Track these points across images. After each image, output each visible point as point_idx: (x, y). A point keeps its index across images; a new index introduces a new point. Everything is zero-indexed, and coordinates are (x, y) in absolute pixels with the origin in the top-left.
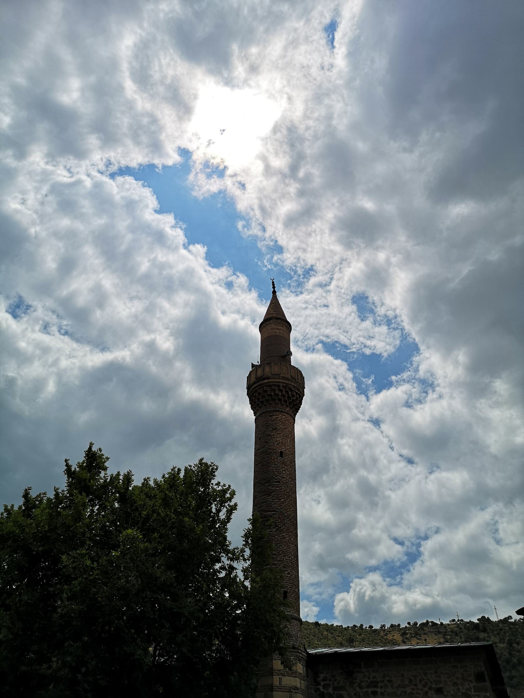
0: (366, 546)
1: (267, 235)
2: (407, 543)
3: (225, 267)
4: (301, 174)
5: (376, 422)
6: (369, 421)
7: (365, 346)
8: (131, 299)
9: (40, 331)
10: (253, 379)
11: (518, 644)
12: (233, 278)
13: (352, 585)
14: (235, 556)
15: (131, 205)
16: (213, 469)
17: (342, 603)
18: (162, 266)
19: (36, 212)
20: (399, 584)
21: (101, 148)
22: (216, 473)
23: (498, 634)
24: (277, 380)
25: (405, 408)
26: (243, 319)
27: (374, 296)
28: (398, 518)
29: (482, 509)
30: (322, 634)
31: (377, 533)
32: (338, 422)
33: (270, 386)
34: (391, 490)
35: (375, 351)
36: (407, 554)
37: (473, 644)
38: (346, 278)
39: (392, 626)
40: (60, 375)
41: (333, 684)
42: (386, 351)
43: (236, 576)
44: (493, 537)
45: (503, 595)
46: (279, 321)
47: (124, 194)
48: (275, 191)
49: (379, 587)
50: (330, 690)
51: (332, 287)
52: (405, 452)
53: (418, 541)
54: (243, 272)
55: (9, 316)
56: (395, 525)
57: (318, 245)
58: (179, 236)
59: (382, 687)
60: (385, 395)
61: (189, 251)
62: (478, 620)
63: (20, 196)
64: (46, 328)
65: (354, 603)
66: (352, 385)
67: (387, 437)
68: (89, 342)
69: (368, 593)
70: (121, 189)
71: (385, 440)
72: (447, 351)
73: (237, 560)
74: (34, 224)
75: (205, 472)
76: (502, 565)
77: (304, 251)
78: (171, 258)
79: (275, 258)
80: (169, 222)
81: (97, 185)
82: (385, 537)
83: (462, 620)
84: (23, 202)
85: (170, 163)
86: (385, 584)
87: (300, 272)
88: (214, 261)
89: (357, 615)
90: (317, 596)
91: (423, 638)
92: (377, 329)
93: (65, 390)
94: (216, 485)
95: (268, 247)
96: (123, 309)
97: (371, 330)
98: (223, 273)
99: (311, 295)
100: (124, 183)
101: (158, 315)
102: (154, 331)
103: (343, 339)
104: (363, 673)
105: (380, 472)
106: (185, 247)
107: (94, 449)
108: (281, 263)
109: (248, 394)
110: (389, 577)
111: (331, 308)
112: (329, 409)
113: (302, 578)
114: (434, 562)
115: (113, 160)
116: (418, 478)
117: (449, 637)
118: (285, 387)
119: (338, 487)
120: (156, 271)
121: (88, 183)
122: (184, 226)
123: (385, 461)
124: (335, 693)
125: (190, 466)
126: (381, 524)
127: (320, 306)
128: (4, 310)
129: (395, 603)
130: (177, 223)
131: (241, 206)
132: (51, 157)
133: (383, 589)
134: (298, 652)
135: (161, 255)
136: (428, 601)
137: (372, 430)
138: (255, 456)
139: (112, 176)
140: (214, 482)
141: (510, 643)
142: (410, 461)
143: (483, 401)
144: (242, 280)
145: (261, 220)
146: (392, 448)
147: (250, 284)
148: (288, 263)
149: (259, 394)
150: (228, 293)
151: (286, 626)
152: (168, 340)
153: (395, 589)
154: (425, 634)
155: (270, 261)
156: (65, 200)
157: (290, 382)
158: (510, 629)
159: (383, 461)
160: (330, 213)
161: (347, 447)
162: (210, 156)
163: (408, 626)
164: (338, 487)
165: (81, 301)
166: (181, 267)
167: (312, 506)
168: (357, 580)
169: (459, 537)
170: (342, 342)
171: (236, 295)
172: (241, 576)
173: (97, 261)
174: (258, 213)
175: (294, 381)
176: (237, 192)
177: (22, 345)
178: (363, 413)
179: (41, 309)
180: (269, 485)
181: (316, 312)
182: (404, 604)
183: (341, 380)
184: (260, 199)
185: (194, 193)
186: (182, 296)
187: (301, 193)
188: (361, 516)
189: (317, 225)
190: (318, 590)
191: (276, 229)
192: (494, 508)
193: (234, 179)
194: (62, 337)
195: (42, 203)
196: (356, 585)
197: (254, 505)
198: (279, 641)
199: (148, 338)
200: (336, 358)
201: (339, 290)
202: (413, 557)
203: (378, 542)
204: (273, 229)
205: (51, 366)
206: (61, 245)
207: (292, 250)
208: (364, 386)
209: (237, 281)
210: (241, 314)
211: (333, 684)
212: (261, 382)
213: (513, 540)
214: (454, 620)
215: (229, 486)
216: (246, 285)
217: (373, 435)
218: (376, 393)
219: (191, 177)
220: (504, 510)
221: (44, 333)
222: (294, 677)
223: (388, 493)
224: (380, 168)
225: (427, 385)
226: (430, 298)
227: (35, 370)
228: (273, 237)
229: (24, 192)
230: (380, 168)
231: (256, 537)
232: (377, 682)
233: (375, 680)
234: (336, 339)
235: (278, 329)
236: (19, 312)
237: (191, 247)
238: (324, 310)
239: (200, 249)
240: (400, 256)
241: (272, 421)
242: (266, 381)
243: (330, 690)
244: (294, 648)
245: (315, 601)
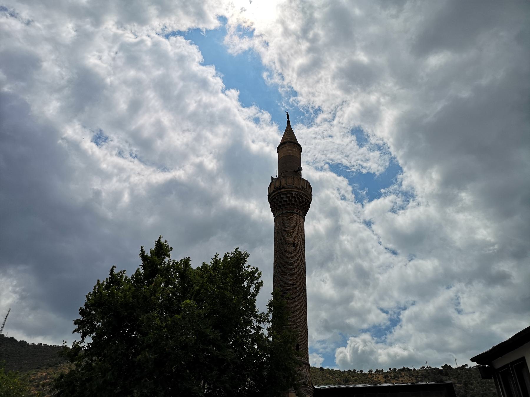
0: (360, 314)
1: (285, 83)
2: (390, 312)
3: (253, 106)
4: (311, 35)
5: (368, 224)
6: (363, 223)
7: (362, 167)
8: (184, 131)
9: (116, 155)
10: (273, 189)
11: (472, 384)
12: (259, 115)
13: (348, 342)
14: (262, 319)
15: (181, 59)
16: (245, 256)
17: (341, 355)
18: (207, 106)
19: (110, 65)
20: (384, 342)
21: (158, 16)
22: (247, 259)
23: (457, 377)
25: (390, 213)
26: (268, 145)
27: (367, 129)
28: (384, 294)
29: (448, 288)
30: (325, 376)
31: (369, 305)
32: (340, 223)
33: (286, 194)
34: (379, 273)
35: (370, 171)
36: (391, 320)
37: (438, 383)
38: (346, 116)
39: (377, 371)
40: (132, 190)
42: (378, 171)
43: (262, 333)
44: (455, 309)
45: (462, 350)
47: (177, 51)
48: (291, 47)
49: (369, 344)
51: (335, 122)
52: (390, 246)
53: (399, 311)
54: (266, 110)
55: (94, 145)
56: (382, 298)
57: (323, 90)
58: (218, 83)
60: (376, 203)
61: (227, 95)
62: (442, 367)
63: (97, 54)
64: (120, 154)
65: (350, 355)
66: (351, 196)
67: (376, 235)
68: (153, 164)
69: (361, 348)
70: (174, 47)
71: (375, 237)
72: (424, 169)
73: (263, 322)
74: (109, 74)
75: (238, 259)
76: (461, 328)
77: (313, 94)
78: (213, 100)
79: (291, 100)
80: (210, 73)
81: (156, 44)
82: (374, 307)
83: (430, 367)
84: (100, 58)
85: (212, 27)
86: (373, 342)
87: (311, 111)
88: (244, 102)
89: (352, 364)
90: (322, 350)
91: (400, 380)
92: (372, 154)
93: (137, 201)
94: (247, 267)
95: (286, 92)
96: (178, 139)
97: (367, 155)
98: (252, 111)
99: (319, 128)
100: (176, 42)
101: (204, 144)
102: (202, 156)
103: (345, 162)
105: (371, 260)
106: (223, 92)
108: (296, 104)
109: (269, 201)
110: (376, 336)
111: (335, 138)
112: (334, 213)
113: (311, 337)
114: (410, 326)
115: (167, 25)
116: (400, 264)
117: (419, 379)
120: (201, 110)
121: (149, 43)
122: (222, 76)
123: (375, 253)
125: (228, 254)
126: (371, 299)
127: (326, 137)
128: (89, 141)
129: (380, 355)
130: (217, 73)
131: (266, 60)
132: (120, 25)
133: (372, 345)
135: (205, 98)
136: (405, 353)
137: (365, 230)
138: (275, 246)
139: (167, 37)
140: (246, 265)
141: (466, 384)
142: (394, 253)
143: (451, 208)
144: (266, 116)
145: (280, 71)
146: (380, 243)
147: (272, 120)
148: (301, 103)
149: (277, 200)
150: (256, 127)
151: (299, 370)
152: (212, 161)
153: (380, 345)
154: (402, 377)
155: (287, 102)
156: (131, 56)
157: (301, 191)
158: (466, 373)
159: (374, 253)
160: (333, 63)
161: (346, 241)
162: (242, 21)
163: (389, 371)
164: (340, 271)
165: (146, 133)
166: (220, 106)
167: (319, 284)
168: (351, 338)
169: (429, 309)
170: (344, 164)
171: (262, 128)
172: (266, 333)
173: (157, 104)
174: (278, 65)
176: (263, 50)
177: (104, 166)
178: (359, 218)
179: (116, 139)
180: (285, 268)
181: (323, 141)
182: (387, 356)
183: (343, 192)
184: (279, 54)
185: (230, 51)
186: (221, 129)
187: (310, 50)
188: (357, 293)
189: (323, 73)
190: (324, 345)
191: (292, 78)
192: (457, 286)
193: (260, 38)
194: (133, 160)
195: (114, 59)
196: (352, 342)
197: (275, 282)
198: (294, 380)
199: (198, 160)
200: (339, 175)
201: (340, 125)
202: (395, 322)
203: (369, 311)
204: (290, 78)
205: (125, 181)
206: (130, 90)
207: (304, 95)
208: (359, 196)
209: (263, 117)
210: (264, 142)
212: (279, 191)
213: (470, 310)
214: (424, 367)
215: (257, 269)
216: (269, 120)
217: (366, 233)
219: (227, 38)
220: (465, 288)
221: (119, 156)
223: (377, 276)
224: (373, 29)
225: (408, 196)
226: (411, 129)
227: (114, 184)
228: (289, 85)
229: (100, 51)
230: (373, 29)
231: (276, 305)
234: (339, 162)
235: (291, 150)
236: (99, 141)
237: (227, 92)
238: (330, 139)
239: (234, 93)
240: (387, 98)
241: (287, 220)
242: (283, 190)
244: (305, 384)
245: (321, 353)
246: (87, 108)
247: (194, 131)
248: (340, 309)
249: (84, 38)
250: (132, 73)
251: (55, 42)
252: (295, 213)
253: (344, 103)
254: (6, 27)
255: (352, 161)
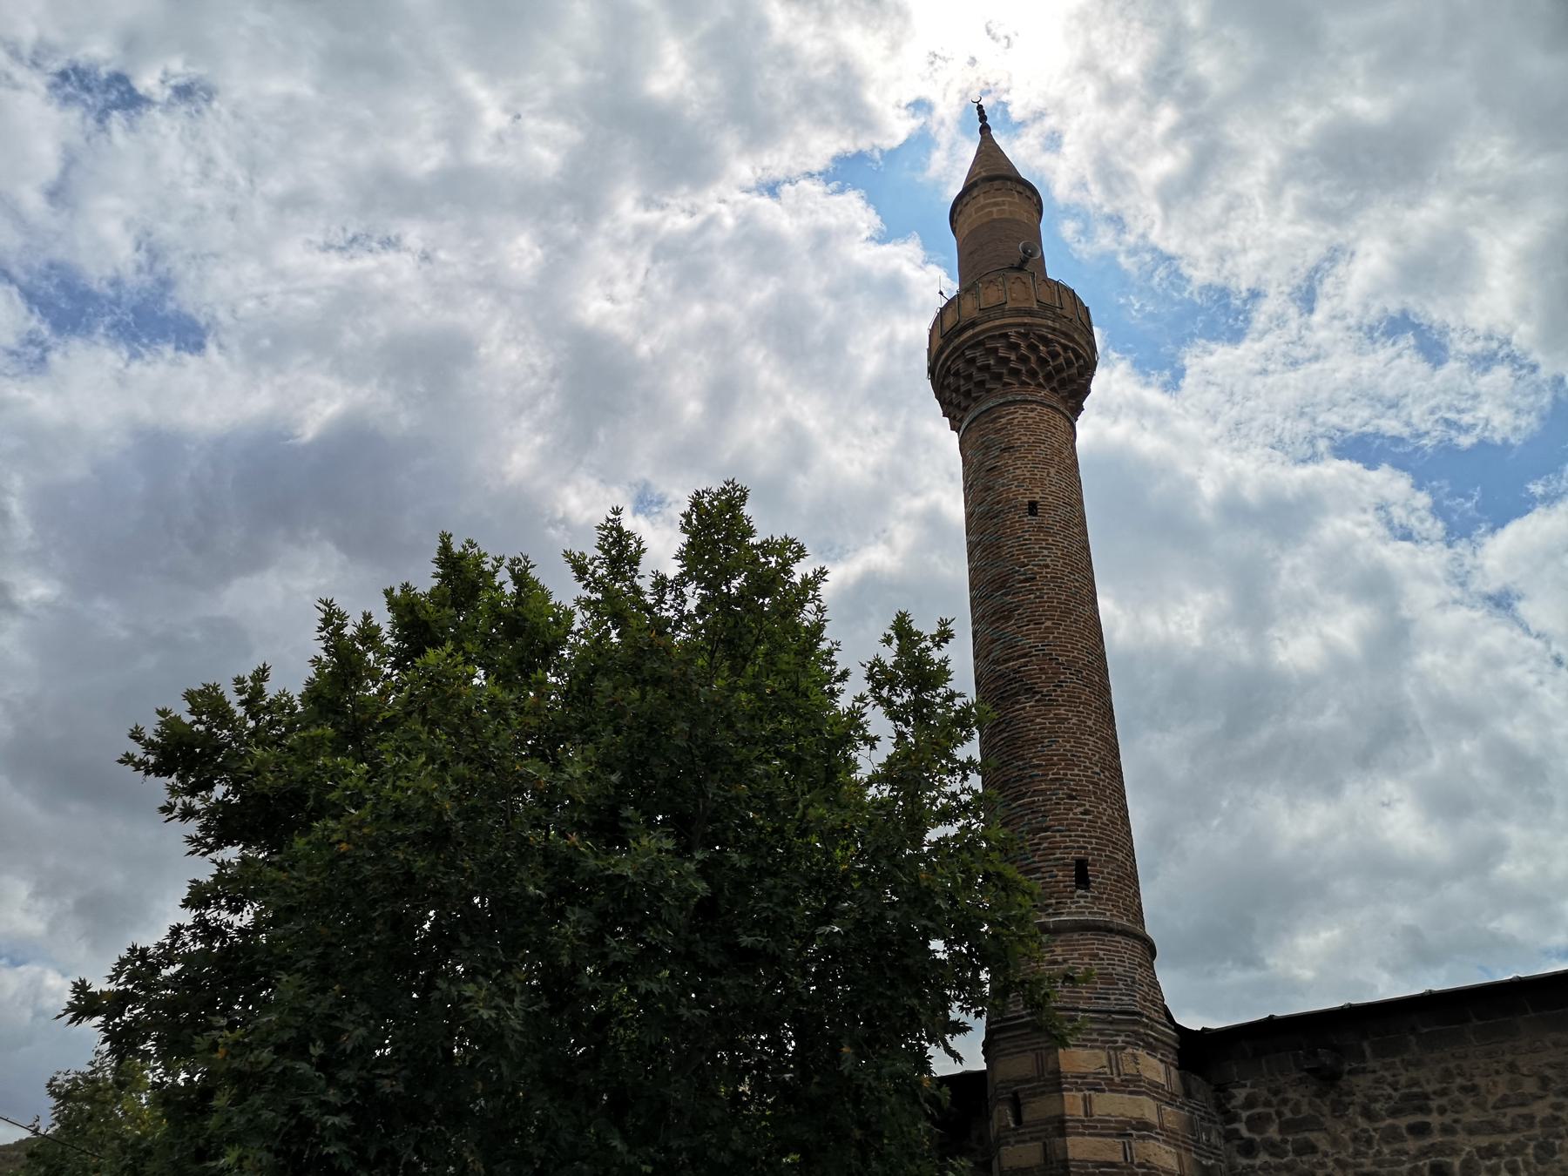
15: (822, 239)
24: (997, 323)
26: (1116, 421)
27: (1436, 312)
33: (981, 343)
41: (1279, 1114)
46: (997, 184)
50: (1273, 1132)
59: (1442, 1111)
103: (1391, 425)
104: (1374, 1072)
107: (457, 549)
118: (1025, 336)
119: (1437, 763)
124: (1290, 1138)
134: (1135, 1022)
156: (685, 264)
157: (1038, 321)
164: (1437, 763)
175: (1049, 314)
180: (1006, 594)
181: (1293, 377)
188: (1512, 832)
200: (1372, 465)
211: (1279, 1114)
212: (957, 342)
218: (1493, 531)
222: (1131, 1093)
232: (1426, 1097)
233: (1415, 1090)
235: (996, 204)
242: (970, 332)
243: (1273, 1132)
246: (601, 435)
247: (889, 428)
248: (1457, 891)
249: (563, 258)
250: (697, 311)
251: (492, 284)
252: (1026, 401)
253: (1336, 254)
254: (380, 280)
255: (1415, 420)
